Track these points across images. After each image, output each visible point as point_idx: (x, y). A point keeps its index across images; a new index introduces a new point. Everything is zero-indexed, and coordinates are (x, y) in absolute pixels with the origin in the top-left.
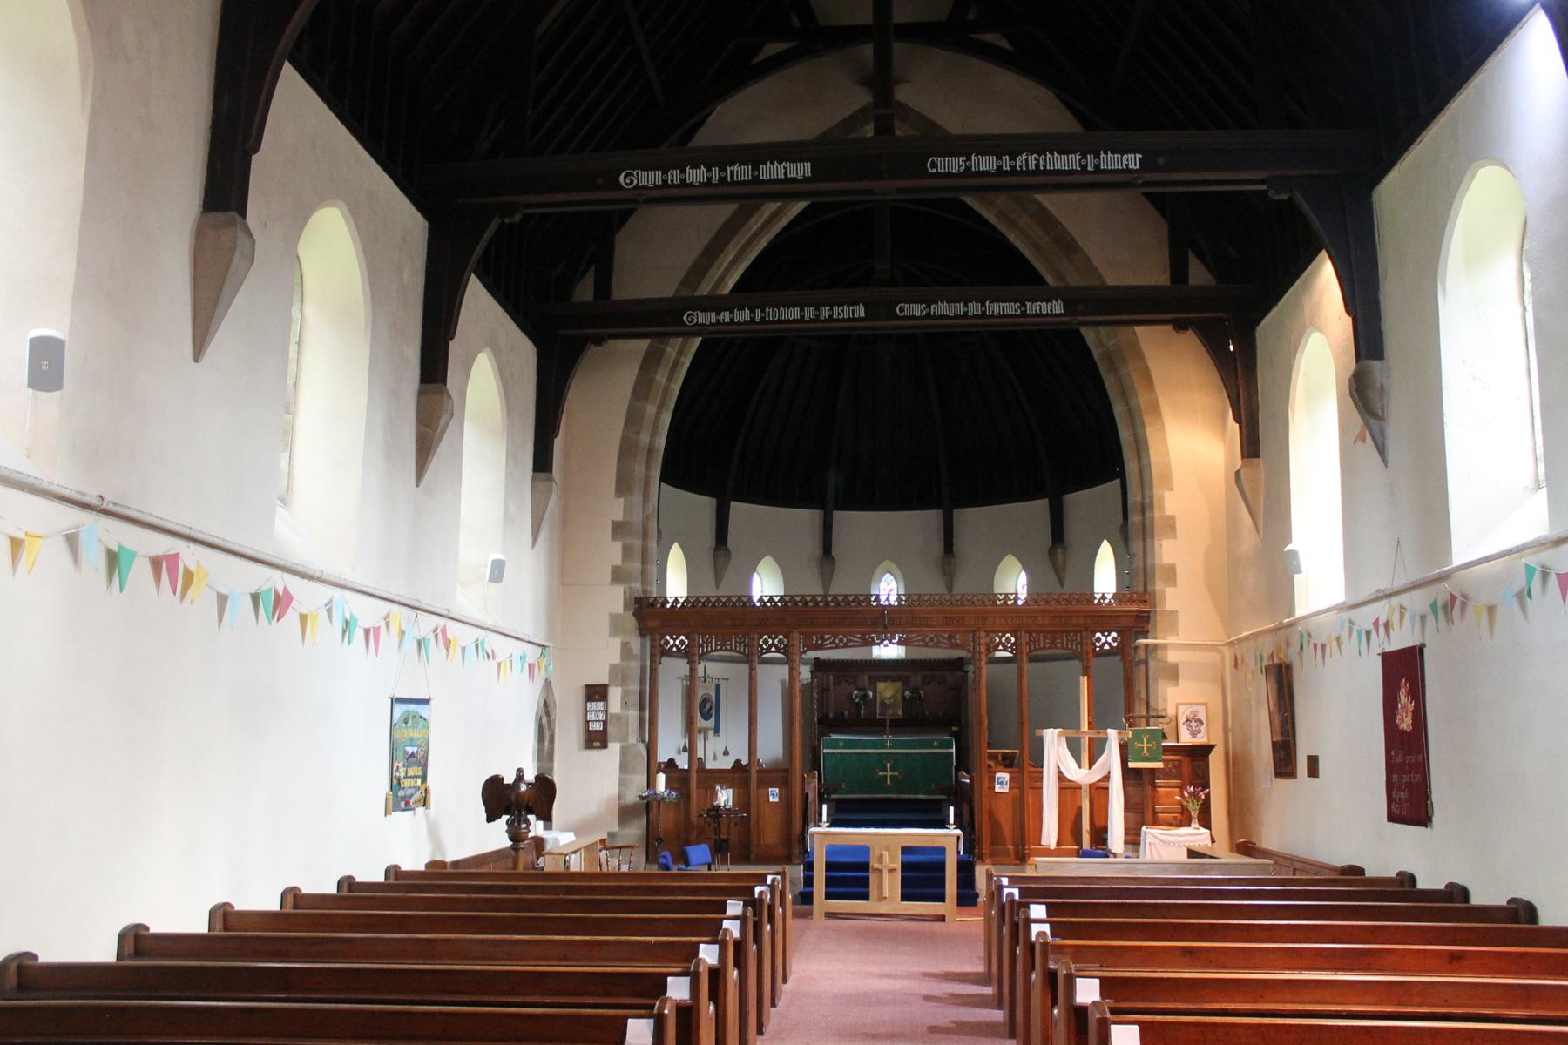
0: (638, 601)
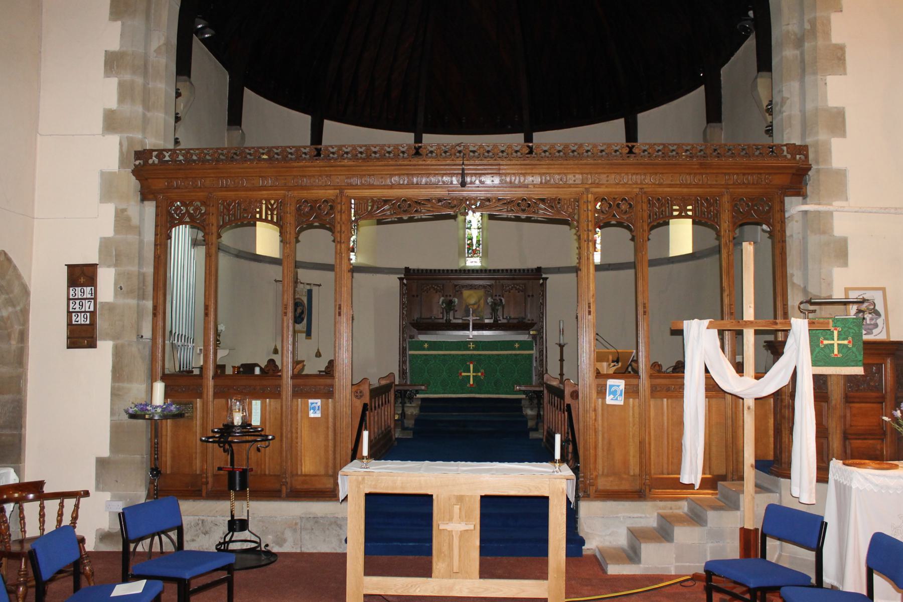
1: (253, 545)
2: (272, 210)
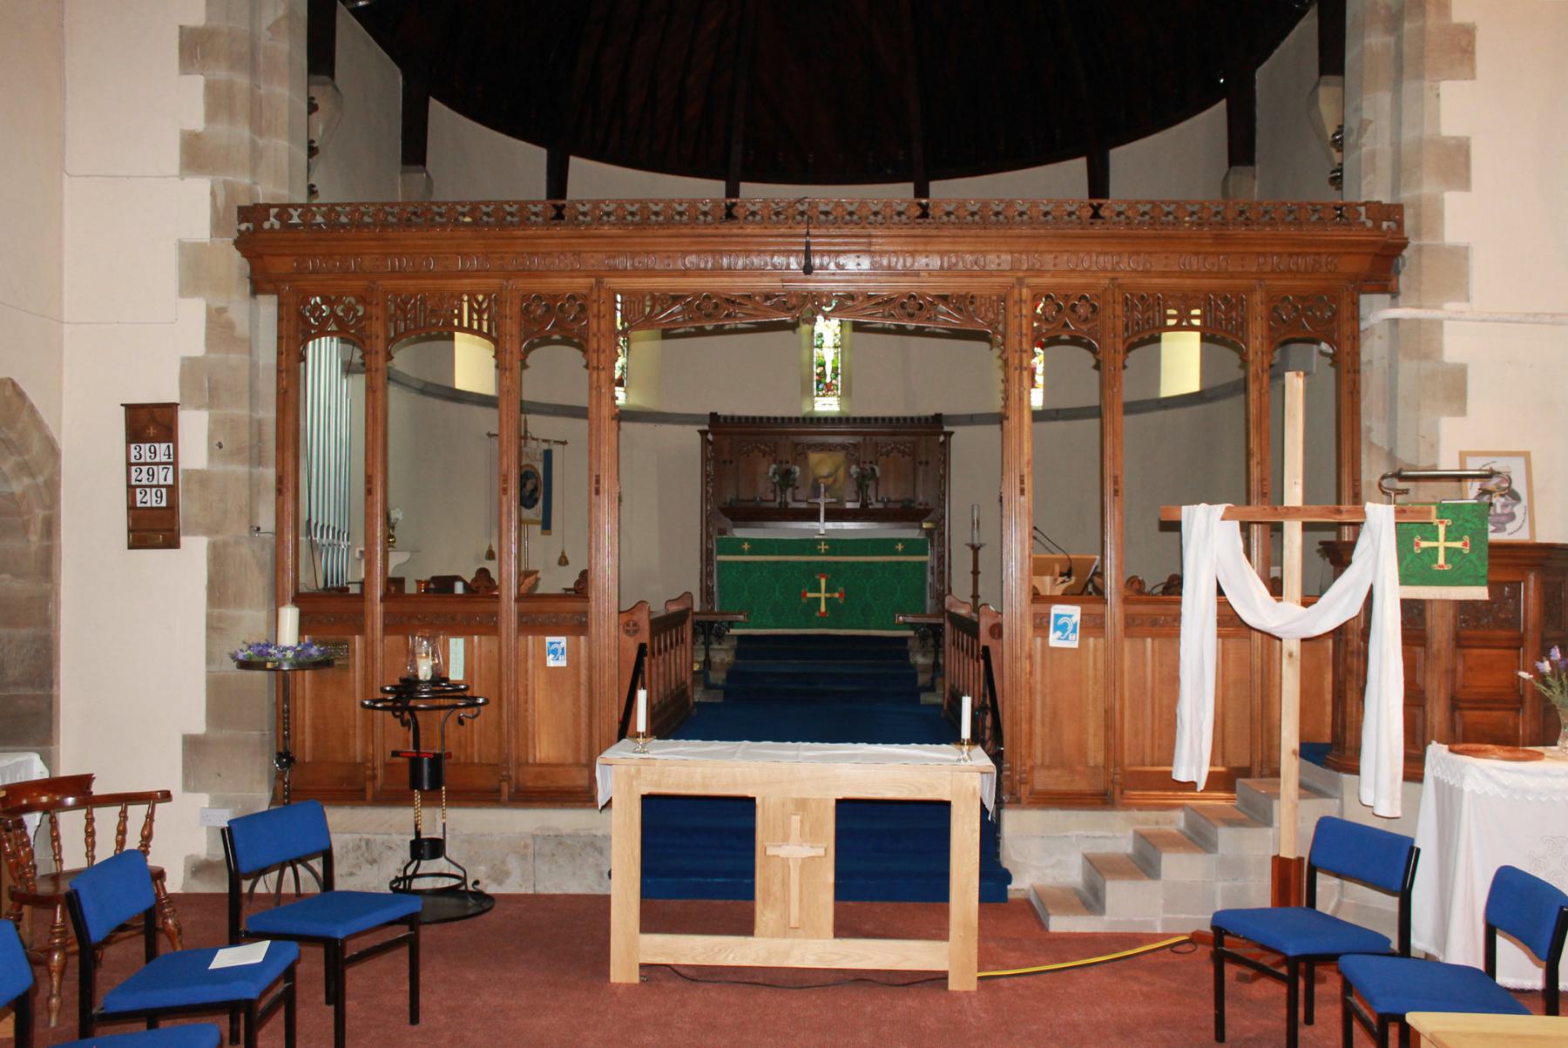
0: (245, 213)
1: (454, 882)
2: (480, 312)
